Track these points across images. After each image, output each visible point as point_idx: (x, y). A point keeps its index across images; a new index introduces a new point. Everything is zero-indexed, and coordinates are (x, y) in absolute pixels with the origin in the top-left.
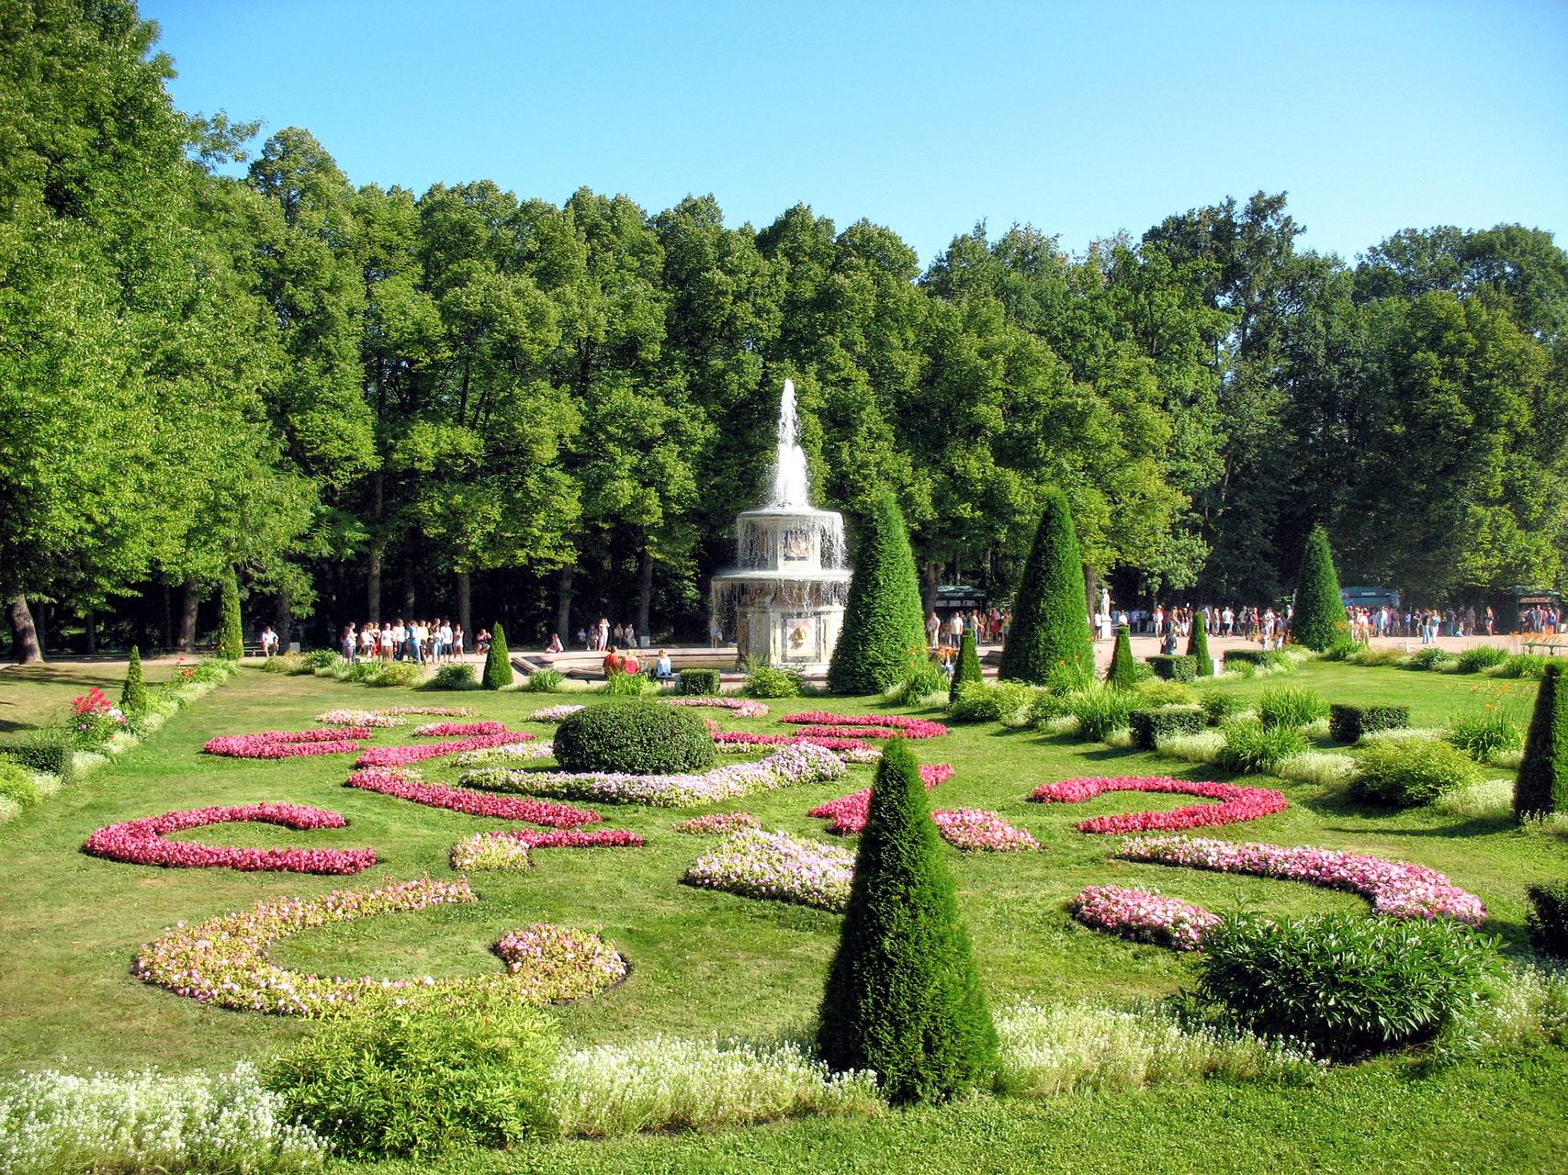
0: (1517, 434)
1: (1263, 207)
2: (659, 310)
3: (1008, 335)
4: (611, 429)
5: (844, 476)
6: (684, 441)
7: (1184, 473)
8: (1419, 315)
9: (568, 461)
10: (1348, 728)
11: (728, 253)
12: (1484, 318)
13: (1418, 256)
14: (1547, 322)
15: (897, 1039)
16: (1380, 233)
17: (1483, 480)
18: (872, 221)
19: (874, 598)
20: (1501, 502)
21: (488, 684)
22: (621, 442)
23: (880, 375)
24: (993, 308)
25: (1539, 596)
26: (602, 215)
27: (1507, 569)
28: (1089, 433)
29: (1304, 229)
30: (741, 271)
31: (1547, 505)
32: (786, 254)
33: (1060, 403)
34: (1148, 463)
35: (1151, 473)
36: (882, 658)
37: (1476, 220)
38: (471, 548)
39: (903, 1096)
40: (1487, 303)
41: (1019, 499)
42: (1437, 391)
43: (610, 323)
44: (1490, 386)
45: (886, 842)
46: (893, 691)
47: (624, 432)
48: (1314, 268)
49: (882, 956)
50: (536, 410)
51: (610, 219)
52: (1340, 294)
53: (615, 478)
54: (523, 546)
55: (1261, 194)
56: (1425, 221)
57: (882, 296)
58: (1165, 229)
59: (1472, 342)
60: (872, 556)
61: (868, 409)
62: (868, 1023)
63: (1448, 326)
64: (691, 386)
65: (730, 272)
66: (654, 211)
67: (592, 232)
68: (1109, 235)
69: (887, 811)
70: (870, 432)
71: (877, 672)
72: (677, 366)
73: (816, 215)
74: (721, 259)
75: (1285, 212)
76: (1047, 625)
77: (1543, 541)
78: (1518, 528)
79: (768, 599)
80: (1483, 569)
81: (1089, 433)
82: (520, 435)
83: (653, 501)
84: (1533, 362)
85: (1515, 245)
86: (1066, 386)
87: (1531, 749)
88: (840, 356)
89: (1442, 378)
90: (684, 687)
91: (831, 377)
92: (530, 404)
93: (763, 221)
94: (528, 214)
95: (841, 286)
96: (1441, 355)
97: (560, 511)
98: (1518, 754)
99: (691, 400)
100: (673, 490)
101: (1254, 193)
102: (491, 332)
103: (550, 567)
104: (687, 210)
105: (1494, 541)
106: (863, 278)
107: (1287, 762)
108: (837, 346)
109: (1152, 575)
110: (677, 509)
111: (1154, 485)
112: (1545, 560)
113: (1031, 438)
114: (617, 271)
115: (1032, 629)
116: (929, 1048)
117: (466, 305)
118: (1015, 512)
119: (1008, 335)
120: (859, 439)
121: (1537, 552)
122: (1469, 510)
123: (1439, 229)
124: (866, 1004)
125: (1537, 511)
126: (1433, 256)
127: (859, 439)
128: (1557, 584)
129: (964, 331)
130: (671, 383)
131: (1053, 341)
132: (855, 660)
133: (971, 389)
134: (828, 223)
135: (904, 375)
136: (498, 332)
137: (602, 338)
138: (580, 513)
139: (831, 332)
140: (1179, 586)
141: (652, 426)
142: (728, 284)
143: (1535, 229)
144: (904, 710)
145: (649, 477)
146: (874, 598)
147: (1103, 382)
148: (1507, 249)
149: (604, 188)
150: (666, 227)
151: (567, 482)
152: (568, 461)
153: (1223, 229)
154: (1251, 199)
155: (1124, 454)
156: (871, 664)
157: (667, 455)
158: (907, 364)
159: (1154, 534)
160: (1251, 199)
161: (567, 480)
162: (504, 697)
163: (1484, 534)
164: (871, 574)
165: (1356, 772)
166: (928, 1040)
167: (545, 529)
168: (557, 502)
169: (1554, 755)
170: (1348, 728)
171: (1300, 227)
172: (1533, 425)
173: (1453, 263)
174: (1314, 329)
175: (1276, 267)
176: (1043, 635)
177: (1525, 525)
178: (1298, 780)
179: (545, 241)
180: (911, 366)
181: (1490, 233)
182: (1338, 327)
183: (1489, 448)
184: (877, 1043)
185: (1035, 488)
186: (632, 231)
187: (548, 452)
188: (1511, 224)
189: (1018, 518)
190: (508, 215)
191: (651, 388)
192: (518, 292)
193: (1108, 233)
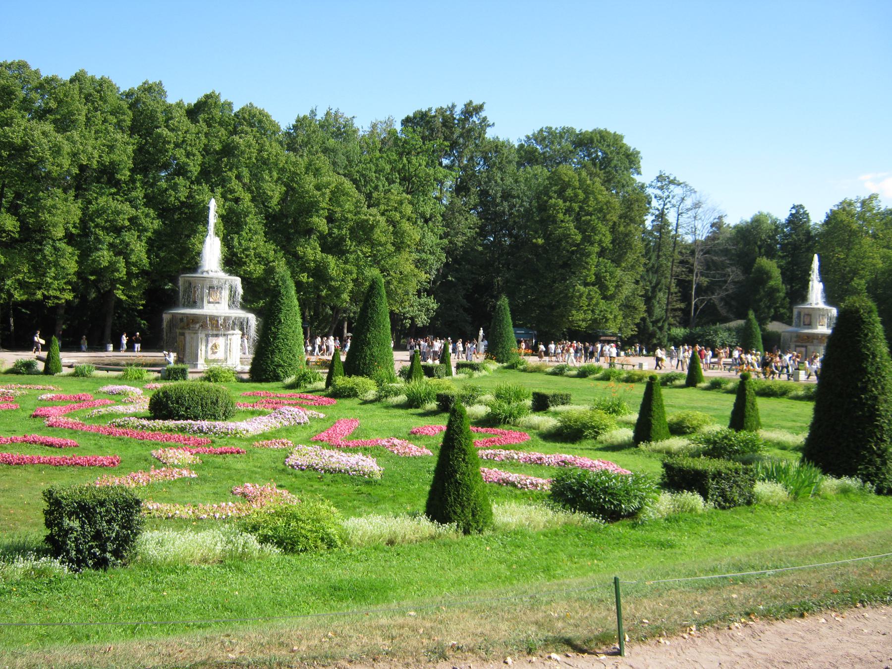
0: (603, 247)
1: (471, 110)
2: (130, 149)
3: (331, 178)
4: (98, 220)
5: (235, 254)
6: (142, 230)
7: (424, 260)
8: (555, 178)
9: (70, 238)
10: (541, 403)
11: (171, 118)
12: (588, 182)
13: (552, 143)
14: (620, 185)
15: (462, 512)
16: (532, 129)
17: (585, 272)
18: (255, 105)
19: (278, 329)
20: (593, 285)
21: (48, 371)
22: (104, 228)
23: (259, 198)
24: (323, 162)
25: (611, 336)
26: (94, 88)
27: (595, 321)
28: (375, 237)
29: (493, 124)
30: (179, 130)
31: (617, 287)
32: (205, 121)
33: (360, 218)
34: (405, 255)
35: (407, 260)
36: (282, 362)
37: (584, 125)
38: (6, 287)
39: (466, 532)
40: (591, 174)
41: (334, 272)
42: (562, 221)
43: (100, 157)
44: (591, 220)
45: (456, 439)
46: (289, 380)
47: (105, 223)
48: (498, 147)
49: (456, 481)
50: (54, 206)
51: (98, 92)
52: (510, 162)
53: (98, 249)
54: (40, 288)
55: (471, 102)
56: (557, 123)
57: (260, 151)
58: (415, 117)
59: (582, 196)
60: (278, 306)
61: (250, 216)
62: (451, 506)
63: (568, 185)
64: (146, 196)
65: (172, 130)
66: (124, 87)
67: (88, 98)
68: (383, 119)
69: (457, 427)
70: (250, 230)
71: (279, 371)
72: (138, 185)
73: (222, 100)
74: (167, 121)
75: (483, 114)
76: (370, 346)
77: (615, 306)
78: (602, 299)
79: (198, 326)
80: (583, 320)
81: (375, 237)
82: (42, 220)
83: (121, 264)
84: (614, 208)
85: (604, 141)
86: (363, 209)
87: (642, 414)
88: (234, 184)
89: (565, 214)
90: (169, 375)
91: (229, 196)
92: (49, 202)
93: (191, 99)
94: (47, 86)
95: (238, 143)
96: (565, 202)
97: (63, 268)
98: (634, 417)
99: (146, 205)
100: (133, 258)
101: (467, 101)
102: (27, 156)
103: (56, 301)
104: (145, 90)
105: (589, 305)
106: (250, 138)
107: (523, 420)
108: (234, 178)
109: (406, 318)
110: (135, 270)
111: (409, 268)
112: (615, 317)
113: (342, 239)
114: (102, 124)
115: (363, 349)
116: (473, 515)
117: (12, 138)
118: (332, 279)
119: (331, 178)
120: (244, 233)
121: (611, 313)
122: (576, 288)
123: (564, 129)
124: (451, 499)
125: (612, 290)
126: (559, 144)
127: (244, 233)
128: (620, 329)
129: (305, 173)
130: (134, 194)
131: (355, 182)
132: (267, 363)
133: (311, 208)
134: (230, 105)
135: (271, 197)
136: (31, 156)
137: (95, 165)
138: (76, 269)
139: (230, 170)
140: (420, 325)
141: (124, 220)
142: (171, 137)
143: (615, 133)
144: (298, 391)
145: (122, 251)
146: (278, 329)
147: (382, 207)
148: (600, 142)
149: (95, 72)
150: (134, 100)
151: (70, 251)
152: (70, 238)
153: (447, 121)
154: (465, 105)
155: (393, 249)
156: (276, 366)
157: (130, 237)
158: (273, 191)
159: (408, 294)
160: (465, 105)
161: (70, 249)
162: (60, 379)
163: (584, 301)
164: (276, 316)
165: (559, 424)
166: (473, 512)
167: (55, 278)
168: (63, 262)
169: (651, 416)
170: (541, 403)
171: (491, 123)
172: (611, 243)
173: (571, 148)
174: (496, 182)
175: (477, 145)
176: (369, 352)
177: (605, 298)
178: (530, 427)
179: (60, 102)
180: (275, 192)
181: (591, 133)
182: (509, 181)
183: (588, 255)
184: (455, 513)
185: (343, 266)
186: (112, 100)
187: (60, 233)
188: (602, 129)
189: (333, 283)
190: (35, 83)
191: (122, 197)
192: (44, 133)
193: (382, 117)
